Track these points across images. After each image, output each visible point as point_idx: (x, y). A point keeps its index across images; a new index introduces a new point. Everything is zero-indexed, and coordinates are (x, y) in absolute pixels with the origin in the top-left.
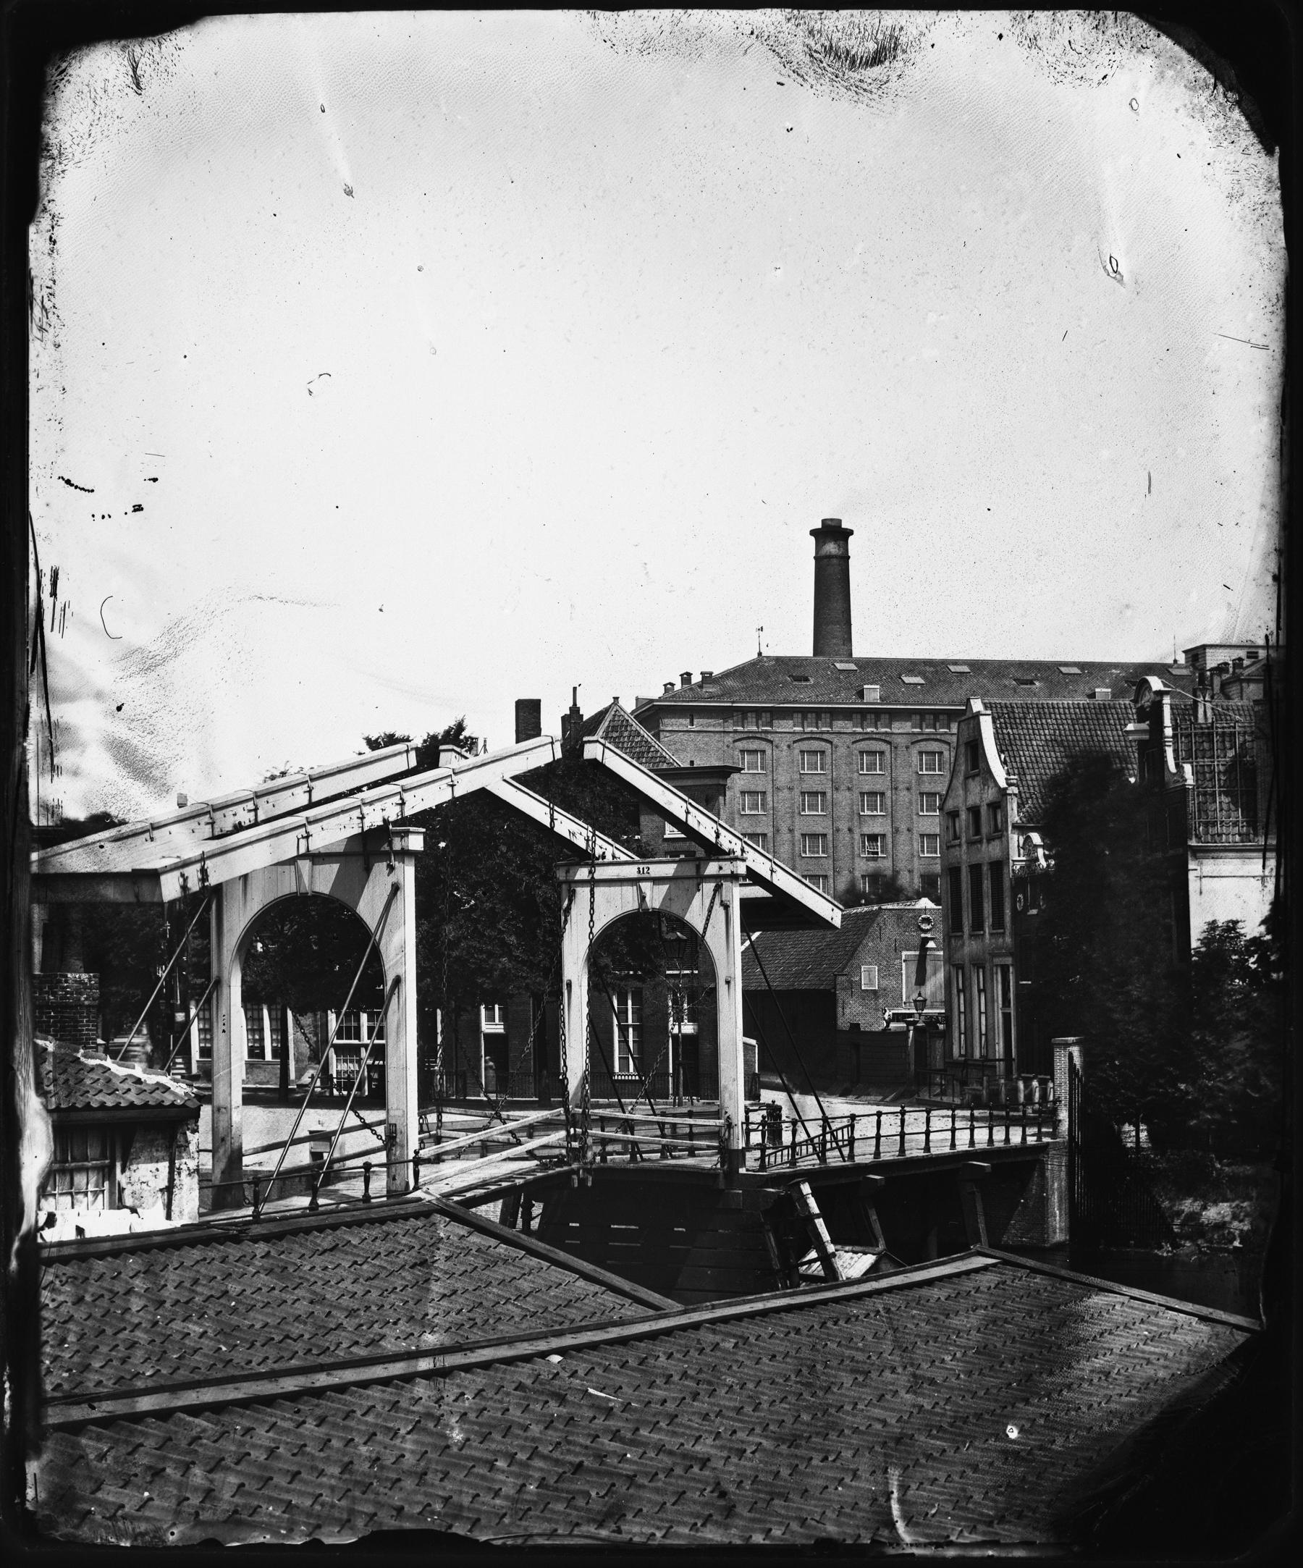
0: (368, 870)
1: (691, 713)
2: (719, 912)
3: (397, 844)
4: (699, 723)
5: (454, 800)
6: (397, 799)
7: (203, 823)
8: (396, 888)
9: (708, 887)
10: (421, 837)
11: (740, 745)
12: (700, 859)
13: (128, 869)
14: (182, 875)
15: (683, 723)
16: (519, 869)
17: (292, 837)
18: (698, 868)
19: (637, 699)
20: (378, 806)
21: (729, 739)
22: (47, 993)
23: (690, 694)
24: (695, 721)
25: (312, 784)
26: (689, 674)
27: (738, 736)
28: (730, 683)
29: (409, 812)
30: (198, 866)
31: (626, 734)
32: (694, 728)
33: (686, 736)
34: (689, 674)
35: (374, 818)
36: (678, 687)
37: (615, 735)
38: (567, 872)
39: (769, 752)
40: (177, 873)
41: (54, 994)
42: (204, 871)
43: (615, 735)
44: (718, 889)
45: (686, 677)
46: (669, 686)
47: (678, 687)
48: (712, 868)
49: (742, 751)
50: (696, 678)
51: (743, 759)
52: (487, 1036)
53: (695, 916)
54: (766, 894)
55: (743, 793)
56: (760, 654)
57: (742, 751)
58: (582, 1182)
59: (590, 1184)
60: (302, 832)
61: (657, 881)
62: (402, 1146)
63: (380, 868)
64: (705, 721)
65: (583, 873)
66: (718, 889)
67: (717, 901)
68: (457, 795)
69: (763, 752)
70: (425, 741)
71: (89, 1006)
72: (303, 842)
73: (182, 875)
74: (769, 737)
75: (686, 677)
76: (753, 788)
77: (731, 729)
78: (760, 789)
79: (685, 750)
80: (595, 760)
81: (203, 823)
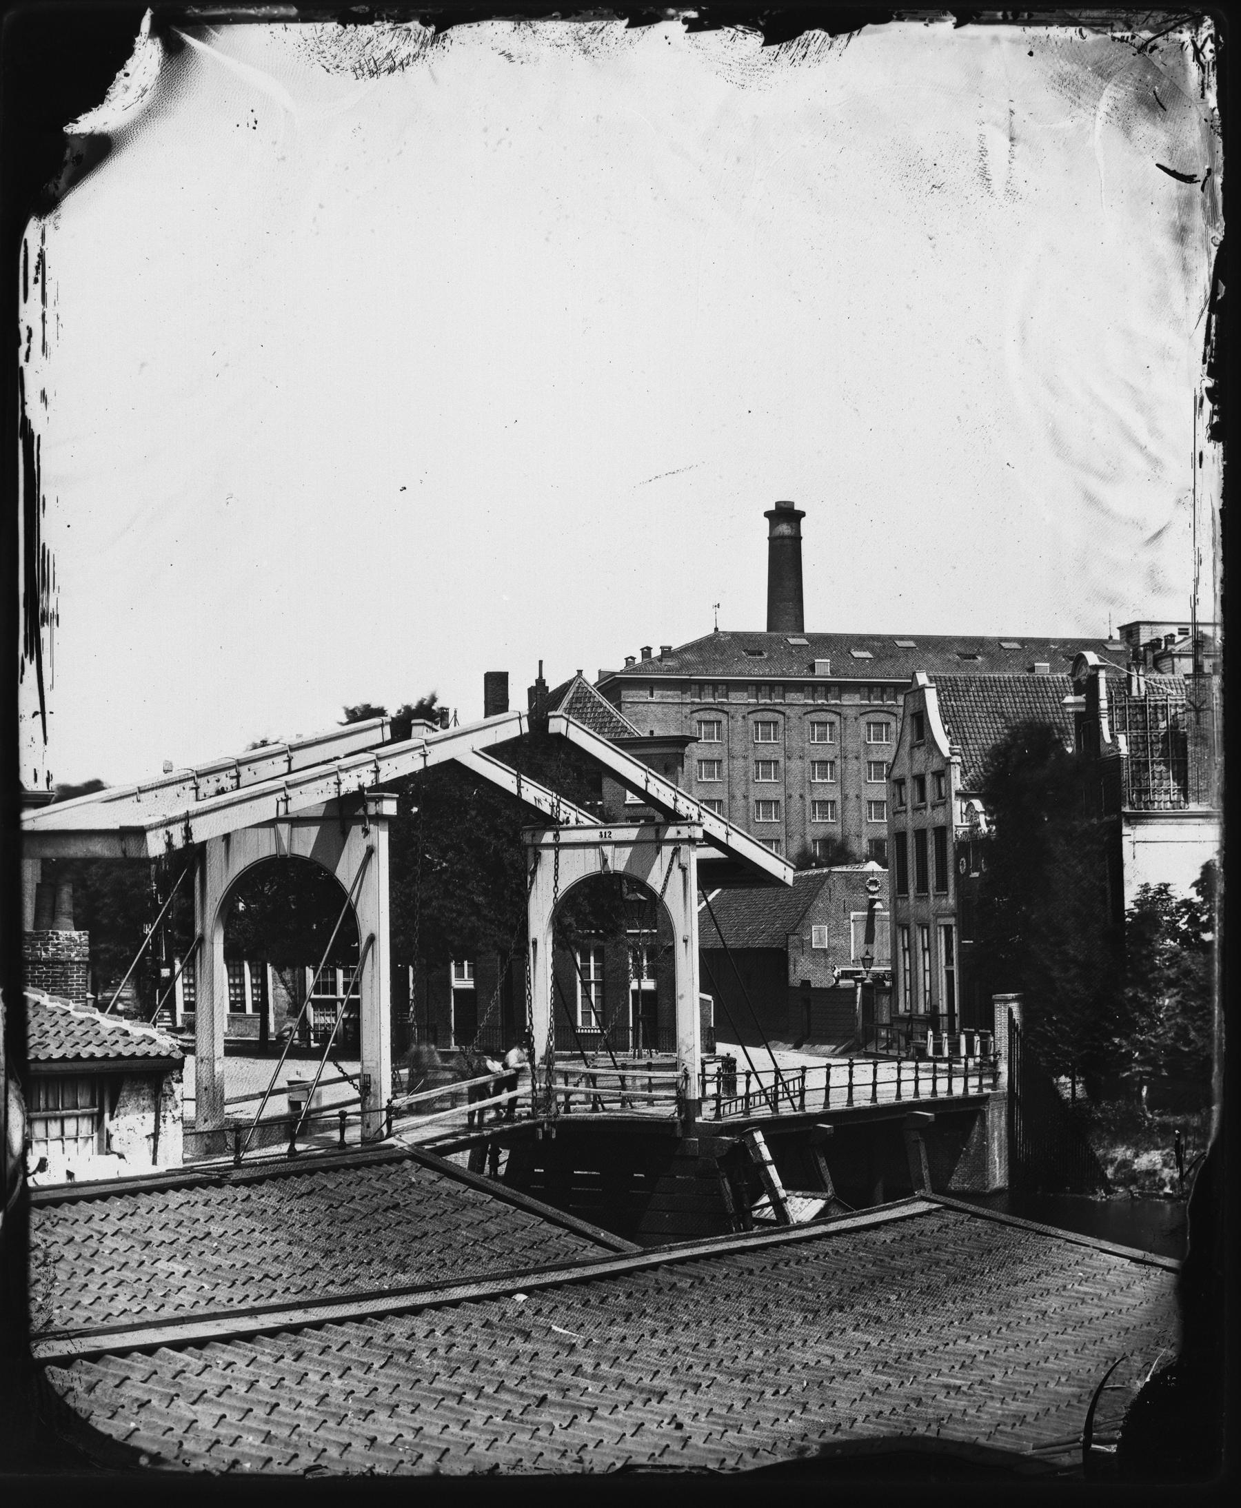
0: (345, 834)
1: (651, 685)
2: (677, 873)
4: (658, 695)
5: (426, 768)
8: (371, 851)
10: (394, 803)
13: (117, 827)
14: (167, 833)
15: (643, 695)
17: (272, 799)
18: (657, 832)
19: (600, 672)
20: (354, 772)
21: (687, 710)
24: (655, 693)
26: (649, 649)
28: (688, 656)
32: (653, 699)
33: (645, 708)
34: (649, 649)
36: (639, 660)
37: (579, 706)
38: (533, 836)
39: (724, 722)
41: (46, 950)
43: (579, 706)
45: (646, 652)
46: (630, 660)
47: (639, 660)
48: (671, 833)
49: (700, 722)
50: (656, 653)
52: (457, 991)
53: (655, 880)
55: (700, 761)
56: (716, 629)
57: (700, 722)
58: (547, 1134)
60: (281, 795)
66: (676, 852)
68: (429, 764)
69: (719, 722)
71: (79, 963)
72: (282, 805)
73: (167, 833)
74: (726, 708)
75: (646, 652)
76: (709, 757)
77: (688, 701)
78: (716, 757)
79: (645, 721)
80: (560, 734)
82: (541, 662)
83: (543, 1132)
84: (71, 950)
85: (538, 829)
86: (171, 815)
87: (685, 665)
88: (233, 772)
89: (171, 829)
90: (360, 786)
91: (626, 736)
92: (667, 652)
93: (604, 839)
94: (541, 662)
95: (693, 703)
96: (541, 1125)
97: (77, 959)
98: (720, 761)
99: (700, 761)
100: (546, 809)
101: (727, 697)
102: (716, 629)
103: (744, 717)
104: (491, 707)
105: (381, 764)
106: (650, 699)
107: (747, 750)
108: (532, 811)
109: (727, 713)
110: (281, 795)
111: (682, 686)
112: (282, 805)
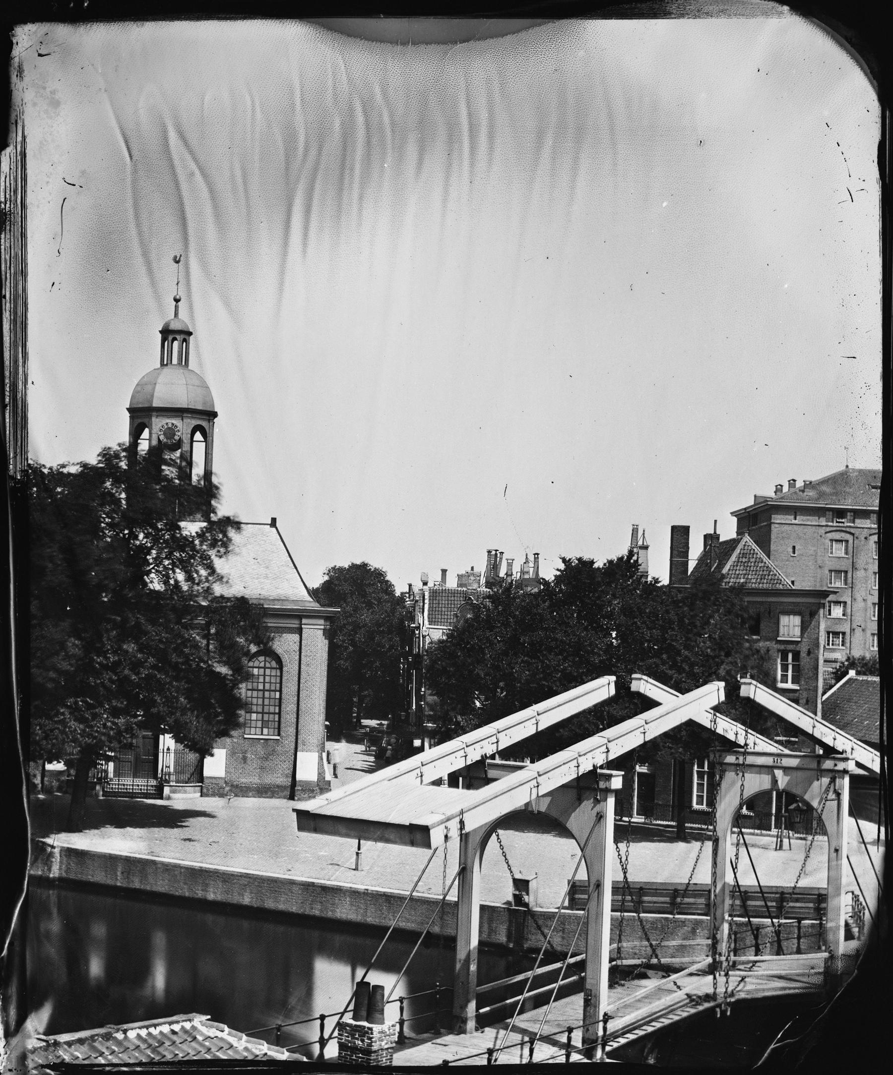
0: (580, 800)
1: (796, 511)
3: (602, 785)
5: (645, 743)
6: (604, 749)
7: (458, 757)
9: (825, 781)
10: (620, 779)
11: (830, 536)
12: (819, 756)
14: (446, 828)
15: (790, 519)
16: (671, 668)
17: (527, 787)
18: (819, 763)
19: (755, 496)
20: (589, 756)
21: (822, 531)
22: (357, 1039)
23: (795, 496)
25: (538, 718)
27: (828, 529)
28: (824, 488)
29: (612, 756)
30: (458, 819)
31: (753, 560)
32: (796, 522)
33: (790, 527)
35: (586, 766)
36: (785, 489)
37: (744, 560)
38: (720, 756)
39: (851, 542)
40: (443, 826)
41: (363, 1041)
42: (462, 822)
43: (744, 560)
44: (833, 780)
46: (779, 489)
48: (828, 764)
49: (832, 540)
50: (799, 484)
51: (832, 546)
52: (640, 774)
54: (866, 773)
55: (831, 571)
56: (847, 466)
57: (832, 540)
58: (723, 1013)
59: (729, 1013)
61: (786, 769)
62: (595, 1007)
63: (587, 804)
64: (805, 518)
65: (730, 759)
66: (833, 780)
67: (832, 789)
68: (647, 739)
69: (847, 541)
70: (605, 564)
71: (387, 1049)
73: (446, 828)
74: (852, 531)
76: (838, 568)
77: (824, 523)
78: (843, 568)
79: (788, 538)
81: (458, 757)
82: (716, 521)
83: (721, 1011)
84: (382, 1041)
85: (724, 751)
86: (449, 814)
87: (822, 495)
88: (494, 739)
89: (449, 824)
90: (594, 766)
91: (781, 587)
92: (809, 485)
93: (775, 764)
94: (716, 521)
95: (827, 526)
96: (719, 1006)
97: (386, 1047)
98: (846, 572)
99: (831, 571)
100: (731, 737)
101: (854, 522)
102: (847, 466)
103: (866, 538)
104: (675, 552)
105: (610, 745)
106: (794, 522)
107: (867, 563)
108: (723, 740)
109: (853, 534)
110: (534, 783)
111: (819, 512)
112: (534, 791)
